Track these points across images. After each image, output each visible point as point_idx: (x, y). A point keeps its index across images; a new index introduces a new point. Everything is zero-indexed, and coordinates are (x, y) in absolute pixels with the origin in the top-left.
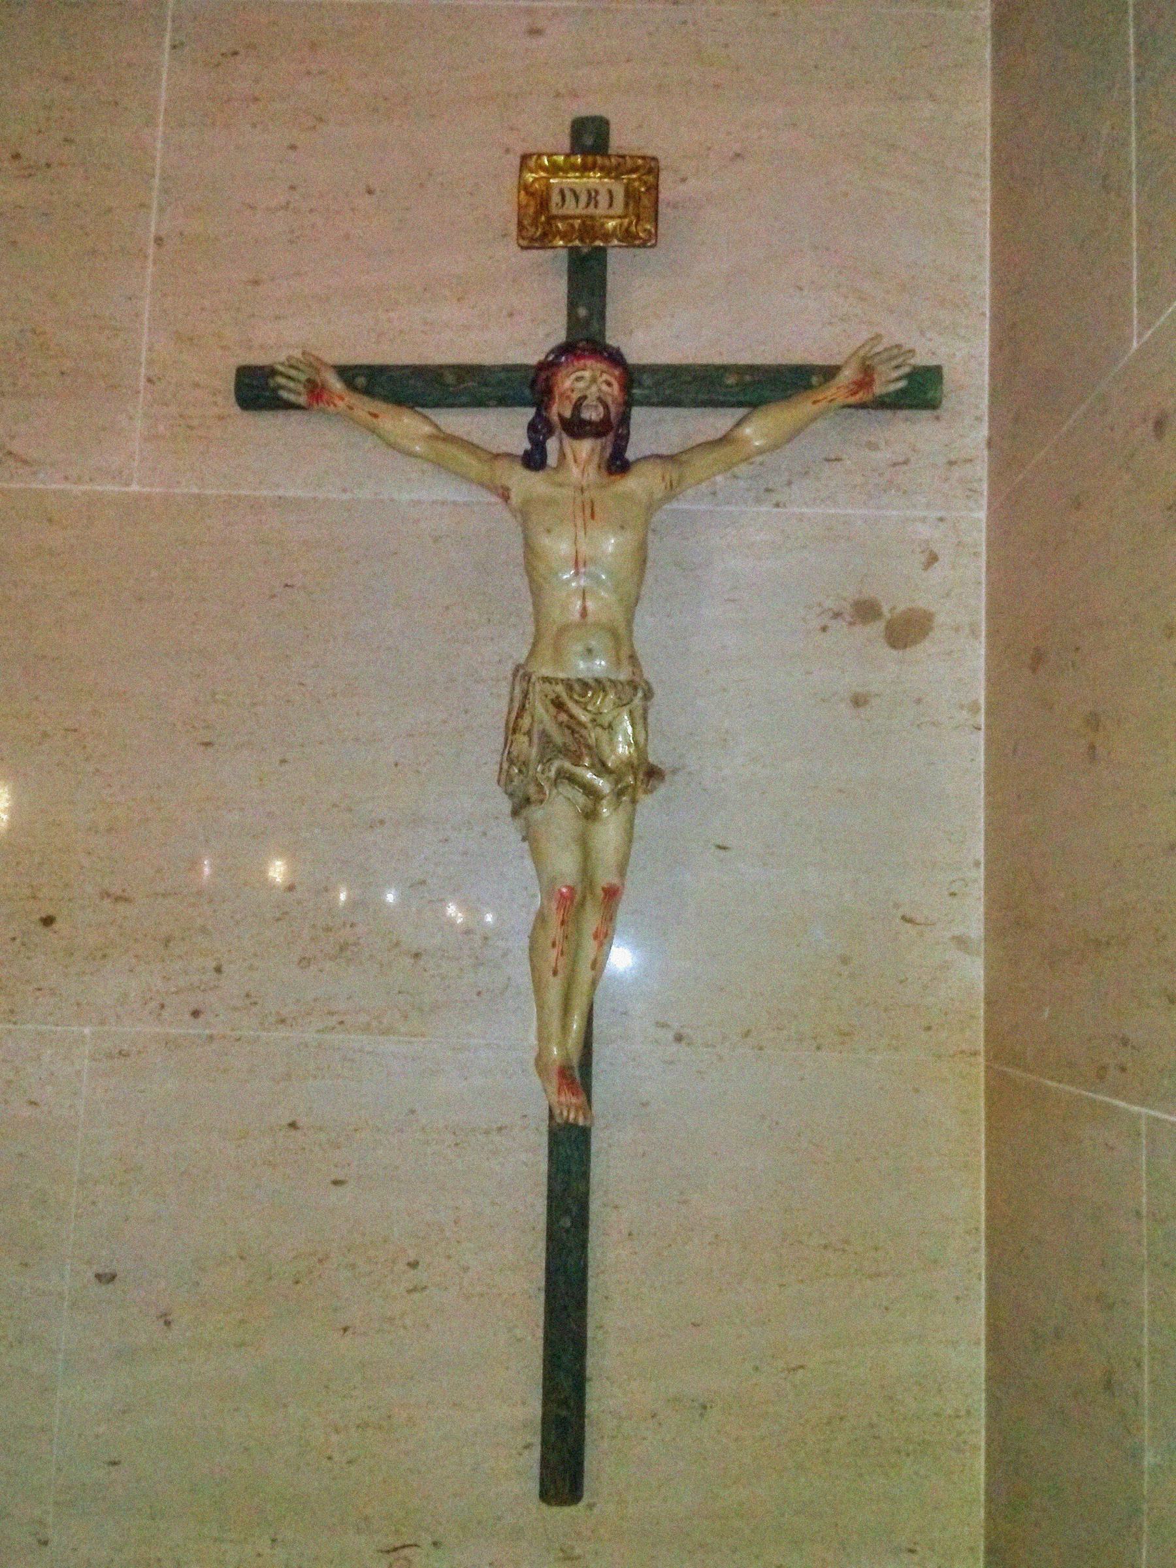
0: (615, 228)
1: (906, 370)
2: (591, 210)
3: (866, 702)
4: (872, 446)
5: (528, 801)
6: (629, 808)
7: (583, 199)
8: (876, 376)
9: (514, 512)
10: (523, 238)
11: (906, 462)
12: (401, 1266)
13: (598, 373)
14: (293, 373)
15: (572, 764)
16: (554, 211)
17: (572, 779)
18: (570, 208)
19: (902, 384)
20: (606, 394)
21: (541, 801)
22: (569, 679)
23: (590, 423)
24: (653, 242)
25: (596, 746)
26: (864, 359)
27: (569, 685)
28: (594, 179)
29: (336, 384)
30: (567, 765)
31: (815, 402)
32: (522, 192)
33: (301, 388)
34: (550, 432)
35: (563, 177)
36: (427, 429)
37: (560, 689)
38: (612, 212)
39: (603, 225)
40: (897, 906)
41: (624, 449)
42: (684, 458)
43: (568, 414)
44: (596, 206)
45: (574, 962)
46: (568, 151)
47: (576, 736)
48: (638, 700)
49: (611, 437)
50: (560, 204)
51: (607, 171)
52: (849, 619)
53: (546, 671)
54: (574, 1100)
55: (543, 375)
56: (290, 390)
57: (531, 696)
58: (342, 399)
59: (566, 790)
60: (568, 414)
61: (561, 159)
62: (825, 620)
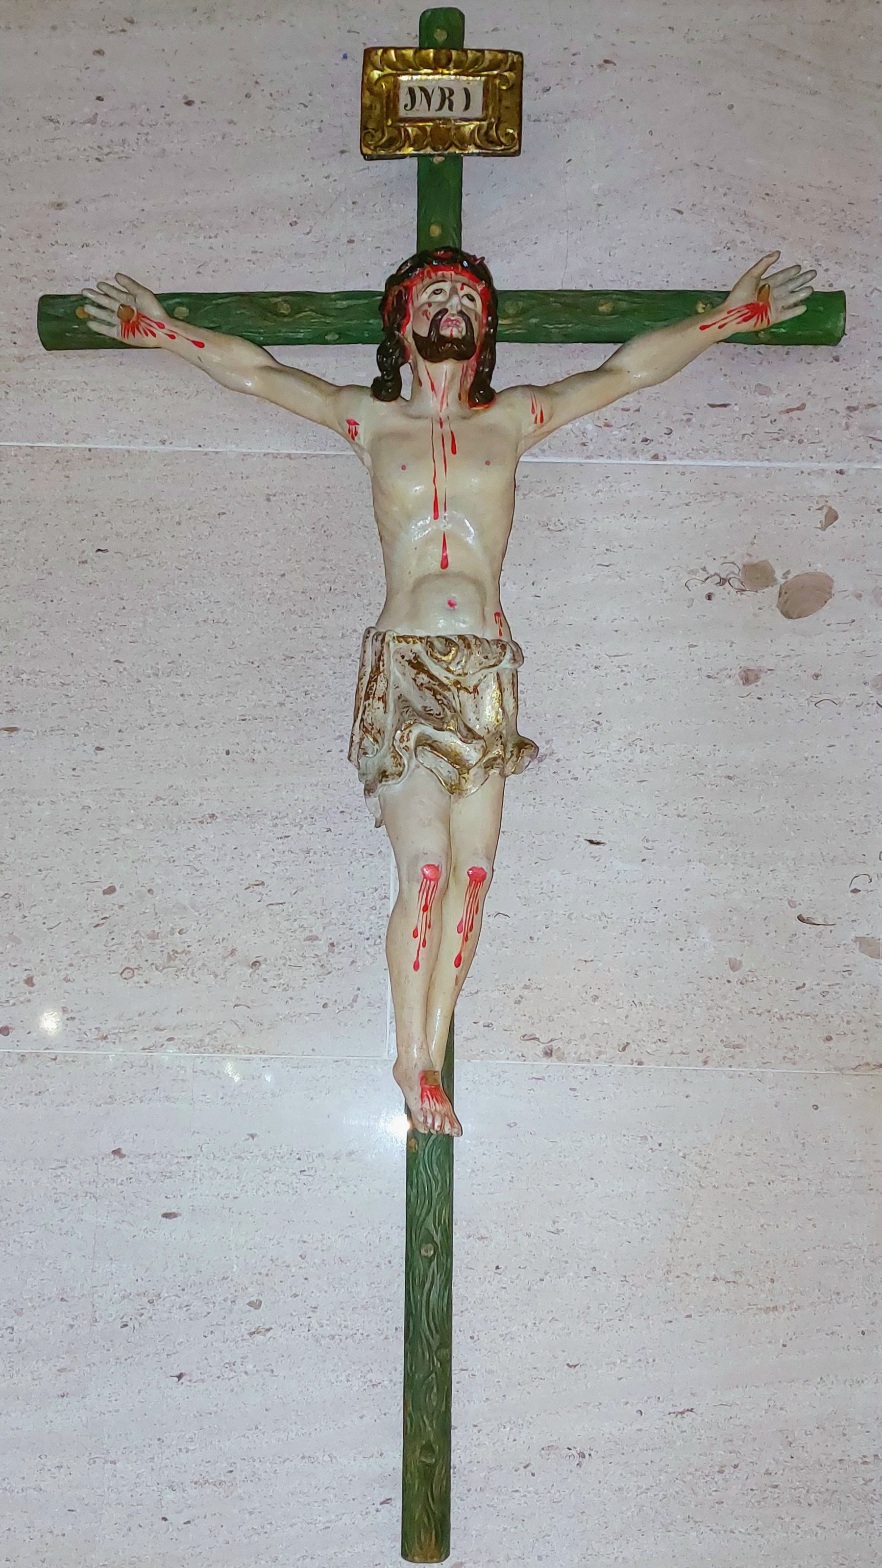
0: (473, 131)
1: (803, 295)
2: (445, 113)
3: (757, 678)
4: (763, 390)
5: (383, 775)
6: (499, 779)
7: (436, 99)
8: (771, 300)
9: (359, 451)
10: (368, 146)
11: (802, 408)
12: (242, 1304)
13: (459, 286)
14: (104, 301)
15: (434, 728)
16: (402, 113)
17: (434, 746)
18: (421, 110)
19: (801, 310)
20: (467, 308)
21: (400, 775)
22: (428, 637)
23: (452, 340)
24: (517, 147)
25: (461, 711)
26: (759, 278)
27: (429, 643)
28: (447, 78)
29: (155, 311)
30: (429, 730)
31: (703, 328)
32: (367, 93)
33: (116, 320)
34: (404, 357)
35: (412, 74)
36: (262, 360)
37: (419, 647)
38: (466, 114)
39: (458, 128)
40: (792, 904)
41: (489, 376)
42: (557, 389)
43: (424, 332)
44: (451, 108)
45: (435, 959)
46: (417, 45)
47: (438, 697)
48: (506, 664)
49: (473, 361)
50: (409, 107)
51: (463, 69)
52: (737, 584)
53: (402, 631)
54: (438, 1107)
55: (395, 290)
56: (102, 322)
57: (385, 658)
58: (162, 326)
59: (428, 758)
60: (424, 332)
61: (410, 53)
62: (710, 587)
